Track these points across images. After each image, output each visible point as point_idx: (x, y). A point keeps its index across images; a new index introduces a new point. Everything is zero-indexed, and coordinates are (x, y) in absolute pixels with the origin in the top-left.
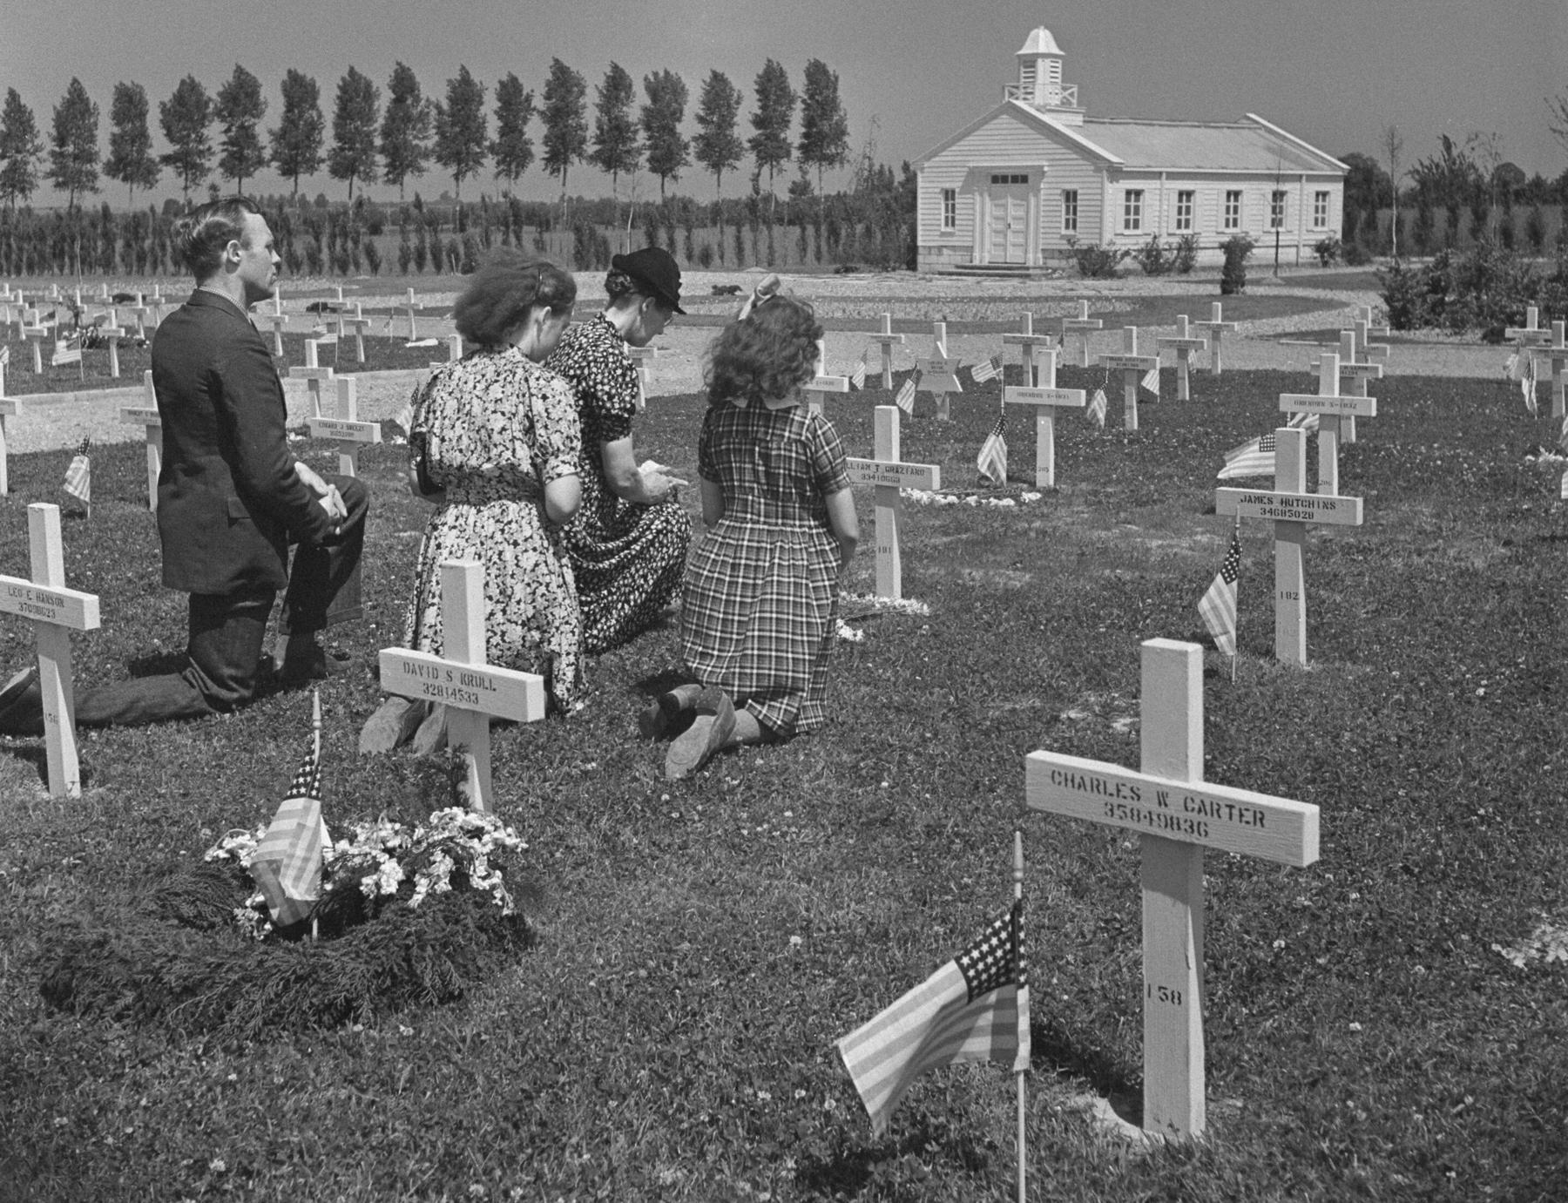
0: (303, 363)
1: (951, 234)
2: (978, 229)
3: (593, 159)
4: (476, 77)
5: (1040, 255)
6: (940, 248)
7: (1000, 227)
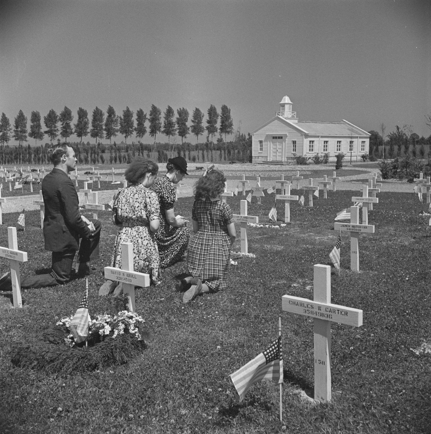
0: (83, 188)
1: (261, 153)
2: (269, 151)
3: (163, 132)
4: (131, 110)
5: (286, 159)
6: (258, 157)
7: (275, 151)
